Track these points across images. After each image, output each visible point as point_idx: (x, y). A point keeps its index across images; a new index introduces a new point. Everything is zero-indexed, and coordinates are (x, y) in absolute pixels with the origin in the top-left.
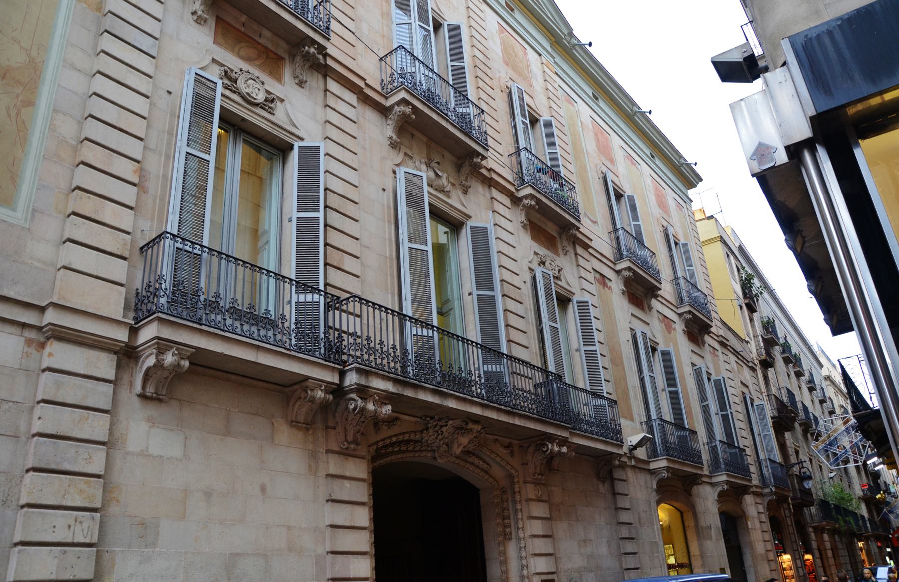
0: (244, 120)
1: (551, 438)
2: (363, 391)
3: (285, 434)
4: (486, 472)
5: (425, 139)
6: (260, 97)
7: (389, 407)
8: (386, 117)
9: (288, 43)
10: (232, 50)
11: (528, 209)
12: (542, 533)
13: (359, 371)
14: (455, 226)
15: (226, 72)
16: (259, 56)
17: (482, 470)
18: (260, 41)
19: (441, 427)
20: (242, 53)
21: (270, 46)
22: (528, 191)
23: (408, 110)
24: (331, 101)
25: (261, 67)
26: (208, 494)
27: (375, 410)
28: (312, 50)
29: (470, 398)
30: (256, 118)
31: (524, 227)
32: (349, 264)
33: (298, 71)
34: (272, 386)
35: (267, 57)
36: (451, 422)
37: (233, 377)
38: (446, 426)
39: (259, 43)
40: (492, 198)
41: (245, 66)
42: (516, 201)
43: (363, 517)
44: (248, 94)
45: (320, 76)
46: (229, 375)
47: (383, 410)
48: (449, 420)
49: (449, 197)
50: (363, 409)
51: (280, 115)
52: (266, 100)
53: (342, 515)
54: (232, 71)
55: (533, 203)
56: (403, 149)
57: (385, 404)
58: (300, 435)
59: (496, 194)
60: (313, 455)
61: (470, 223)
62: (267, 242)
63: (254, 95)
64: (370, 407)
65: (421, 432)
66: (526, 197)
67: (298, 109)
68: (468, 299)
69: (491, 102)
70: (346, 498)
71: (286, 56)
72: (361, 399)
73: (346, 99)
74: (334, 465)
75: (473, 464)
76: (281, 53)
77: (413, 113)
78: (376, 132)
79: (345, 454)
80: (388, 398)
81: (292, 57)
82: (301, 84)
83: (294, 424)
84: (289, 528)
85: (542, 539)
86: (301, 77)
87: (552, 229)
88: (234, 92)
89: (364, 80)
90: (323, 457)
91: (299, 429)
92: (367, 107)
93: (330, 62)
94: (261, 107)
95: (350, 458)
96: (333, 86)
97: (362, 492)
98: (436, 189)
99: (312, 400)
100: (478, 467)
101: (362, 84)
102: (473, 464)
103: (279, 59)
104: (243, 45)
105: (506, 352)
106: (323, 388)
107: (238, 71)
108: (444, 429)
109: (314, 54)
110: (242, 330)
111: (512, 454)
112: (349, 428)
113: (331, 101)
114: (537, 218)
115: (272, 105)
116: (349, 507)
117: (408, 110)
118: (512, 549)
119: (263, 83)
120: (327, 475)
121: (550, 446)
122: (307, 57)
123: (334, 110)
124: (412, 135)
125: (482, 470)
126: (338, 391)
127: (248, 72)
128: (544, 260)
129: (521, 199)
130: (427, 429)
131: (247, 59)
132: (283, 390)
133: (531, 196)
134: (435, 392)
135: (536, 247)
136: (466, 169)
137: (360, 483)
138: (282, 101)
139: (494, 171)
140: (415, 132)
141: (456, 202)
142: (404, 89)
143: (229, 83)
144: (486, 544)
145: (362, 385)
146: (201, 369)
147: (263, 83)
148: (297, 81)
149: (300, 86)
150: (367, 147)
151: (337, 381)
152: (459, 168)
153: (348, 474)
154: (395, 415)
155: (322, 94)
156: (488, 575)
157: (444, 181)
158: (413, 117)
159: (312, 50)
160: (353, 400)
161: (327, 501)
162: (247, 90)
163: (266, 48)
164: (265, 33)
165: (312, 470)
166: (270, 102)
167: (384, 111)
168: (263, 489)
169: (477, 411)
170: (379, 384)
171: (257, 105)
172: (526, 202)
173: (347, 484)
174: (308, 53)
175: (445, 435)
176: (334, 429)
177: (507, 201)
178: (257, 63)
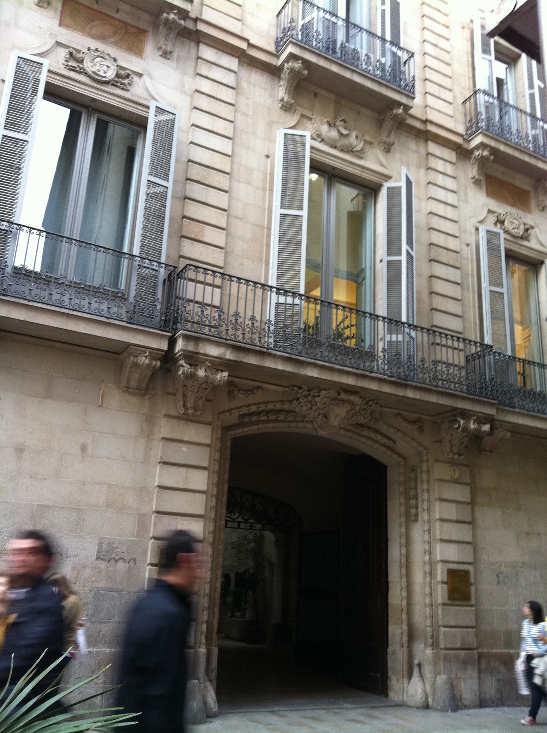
0: (93, 100)
1: (465, 414)
2: (193, 358)
3: (115, 398)
4: (389, 448)
5: (333, 97)
6: (110, 74)
7: (226, 374)
8: (279, 78)
9: (150, 13)
10: (82, 31)
11: (482, 162)
12: (454, 518)
13: (187, 338)
14: (369, 189)
15: (71, 54)
16: (116, 32)
17: (384, 445)
18: (117, 16)
19: (314, 397)
20: (95, 32)
21: (129, 20)
22: (478, 140)
23: (297, 65)
24: (204, 70)
25: (116, 44)
26: (20, 450)
27: (206, 376)
28: (172, 16)
29: (313, 361)
30: (108, 97)
31: (477, 182)
32: (210, 235)
33: (162, 42)
34: (103, 354)
35: (126, 32)
36: (323, 393)
37: (58, 344)
38: (319, 396)
39: (117, 19)
40: (428, 154)
41: (94, 44)
42: (463, 153)
43: (200, 480)
44: (94, 72)
45: (193, 44)
46: (53, 343)
47: (218, 377)
48: (321, 390)
49: (360, 158)
50: (192, 376)
51: (138, 90)
52: (117, 75)
53: (174, 477)
54: (78, 51)
55: (486, 153)
56: (300, 110)
57: (222, 371)
58: (134, 400)
59: (433, 147)
60: (150, 421)
61: (386, 185)
62: (364, 279)
63: (101, 73)
64: (472, 426)
65: (291, 402)
66: (477, 147)
67: (160, 83)
68: (379, 265)
69: (442, 43)
70: (181, 462)
71: (150, 29)
72: (191, 365)
73: (224, 65)
74: (165, 428)
75: (370, 438)
76: (143, 25)
77: (305, 68)
78: (263, 95)
79: (186, 418)
80: (220, 364)
81: (156, 26)
82: (166, 55)
83: (127, 389)
84: (110, 486)
85: (455, 525)
86: (164, 47)
87: (522, 182)
88: (80, 73)
89: (247, 40)
90: (163, 421)
91: (133, 394)
92: (254, 70)
93: (201, 27)
94: (113, 85)
95: (190, 424)
96: (208, 53)
97: (202, 457)
98: (342, 150)
99: (136, 365)
100: (377, 442)
101: (243, 45)
102: (370, 438)
103: (143, 32)
104: (96, 23)
105: (368, 310)
106: (147, 354)
107: (85, 50)
108: (317, 399)
109: (174, 21)
110: (364, 366)
111: (421, 430)
112: (189, 394)
113: (204, 70)
114: (497, 171)
115: (126, 81)
116: (183, 470)
117: (297, 65)
118: (418, 532)
119: (115, 60)
120: (162, 438)
121: (462, 422)
122: (169, 25)
123: (206, 77)
124: (316, 95)
125: (384, 445)
126: (168, 358)
127: (96, 50)
128: (501, 218)
129: (471, 152)
130: (297, 399)
131: (101, 38)
132: (112, 356)
133: (482, 145)
134: (289, 360)
135: (493, 205)
136: (388, 124)
137: (200, 449)
138: (140, 75)
139: (432, 122)
140: (318, 90)
141: (373, 162)
142: (291, 42)
143: (75, 64)
144: (389, 523)
145: (190, 352)
146: (22, 337)
147: (115, 60)
148: (160, 53)
149: (165, 57)
150: (250, 113)
151: (164, 346)
152: (380, 124)
153: (186, 439)
154: (232, 379)
155: (193, 62)
156: (389, 557)
157: (352, 139)
158: (306, 72)
159: (172, 16)
160: (182, 366)
161: (160, 463)
162: (93, 70)
163: (125, 23)
164: (123, 6)
165: (149, 435)
166: (123, 78)
167: (274, 72)
168: (83, 448)
169: (350, 381)
170: (213, 351)
171: (107, 83)
172: (477, 153)
173: (184, 448)
174: (167, 20)
175: (319, 405)
176: (175, 395)
177: (451, 155)
178: (112, 40)
